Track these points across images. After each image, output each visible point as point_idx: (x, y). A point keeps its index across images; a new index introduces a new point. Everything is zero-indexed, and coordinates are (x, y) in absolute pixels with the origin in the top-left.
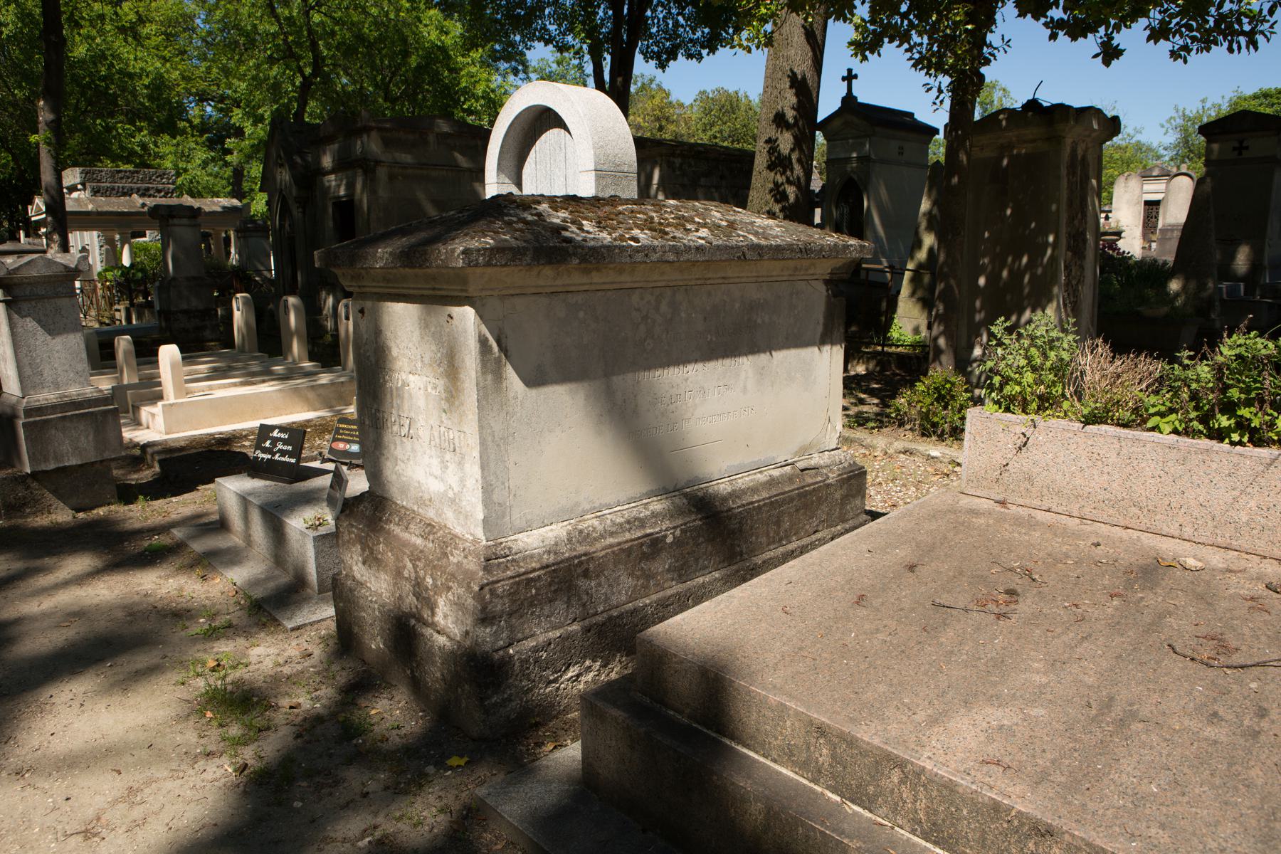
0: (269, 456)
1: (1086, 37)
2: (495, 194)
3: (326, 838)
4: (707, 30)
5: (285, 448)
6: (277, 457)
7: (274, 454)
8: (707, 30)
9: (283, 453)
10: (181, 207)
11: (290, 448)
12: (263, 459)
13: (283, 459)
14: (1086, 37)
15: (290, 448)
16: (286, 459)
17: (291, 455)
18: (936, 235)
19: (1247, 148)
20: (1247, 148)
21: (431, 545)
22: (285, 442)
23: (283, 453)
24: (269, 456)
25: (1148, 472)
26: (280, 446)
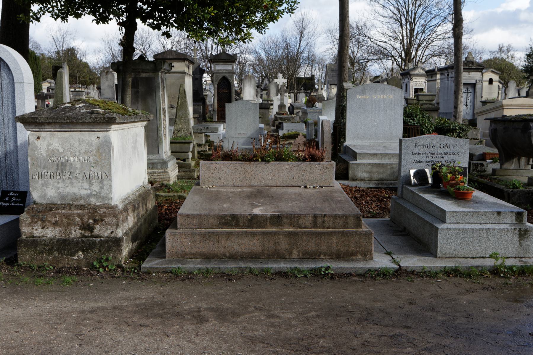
0: (8, 204)
1: (178, 30)
2: (486, 59)
3: (215, 312)
4: (243, 25)
5: (17, 200)
6: (12, 204)
7: (11, 203)
8: (243, 25)
9: (16, 202)
10: (65, 107)
11: (20, 199)
12: (5, 205)
13: (16, 205)
14: (178, 30)
15: (20, 199)
16: (18, 204)
17: (20, 202)
18: (33, 113)
19: (173, 66)
20: (173, 66)
21: (86, 211)
22: (16, 197)
23: (16, 202)
24: (8, 204)
25: (249, 171)
26: (14, 199)
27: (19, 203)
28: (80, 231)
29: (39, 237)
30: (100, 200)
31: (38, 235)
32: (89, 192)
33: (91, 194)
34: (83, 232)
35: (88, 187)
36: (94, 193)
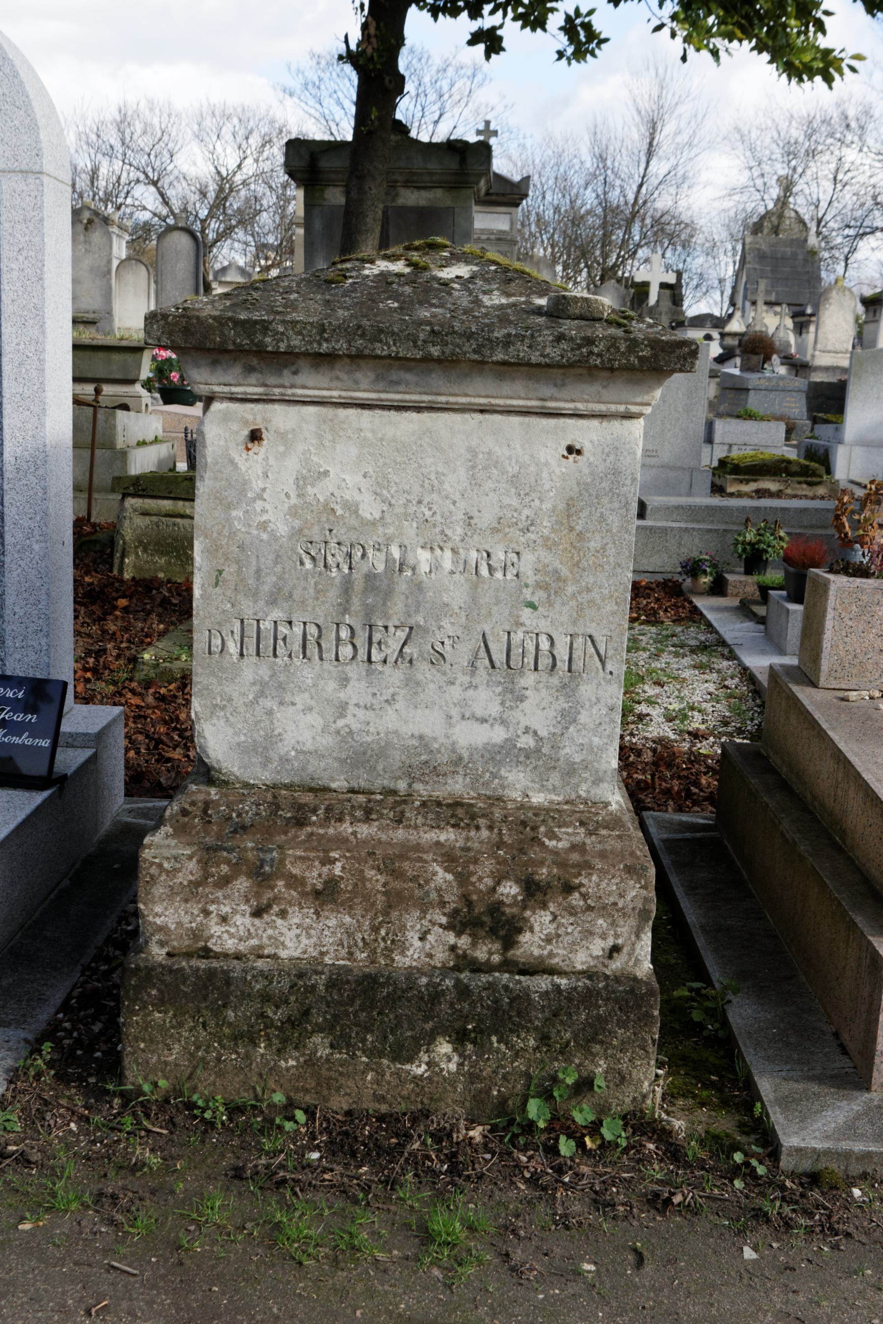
5: (19, 717)
27: (32, 736)
28: (451, 938)
29: (238, 956)
30: (555, 779)
31: (230, 945)
32: (498, 735)
33: (510, 743)
34: (464, 942)
35: (495, 709)
36: (526, 742)
